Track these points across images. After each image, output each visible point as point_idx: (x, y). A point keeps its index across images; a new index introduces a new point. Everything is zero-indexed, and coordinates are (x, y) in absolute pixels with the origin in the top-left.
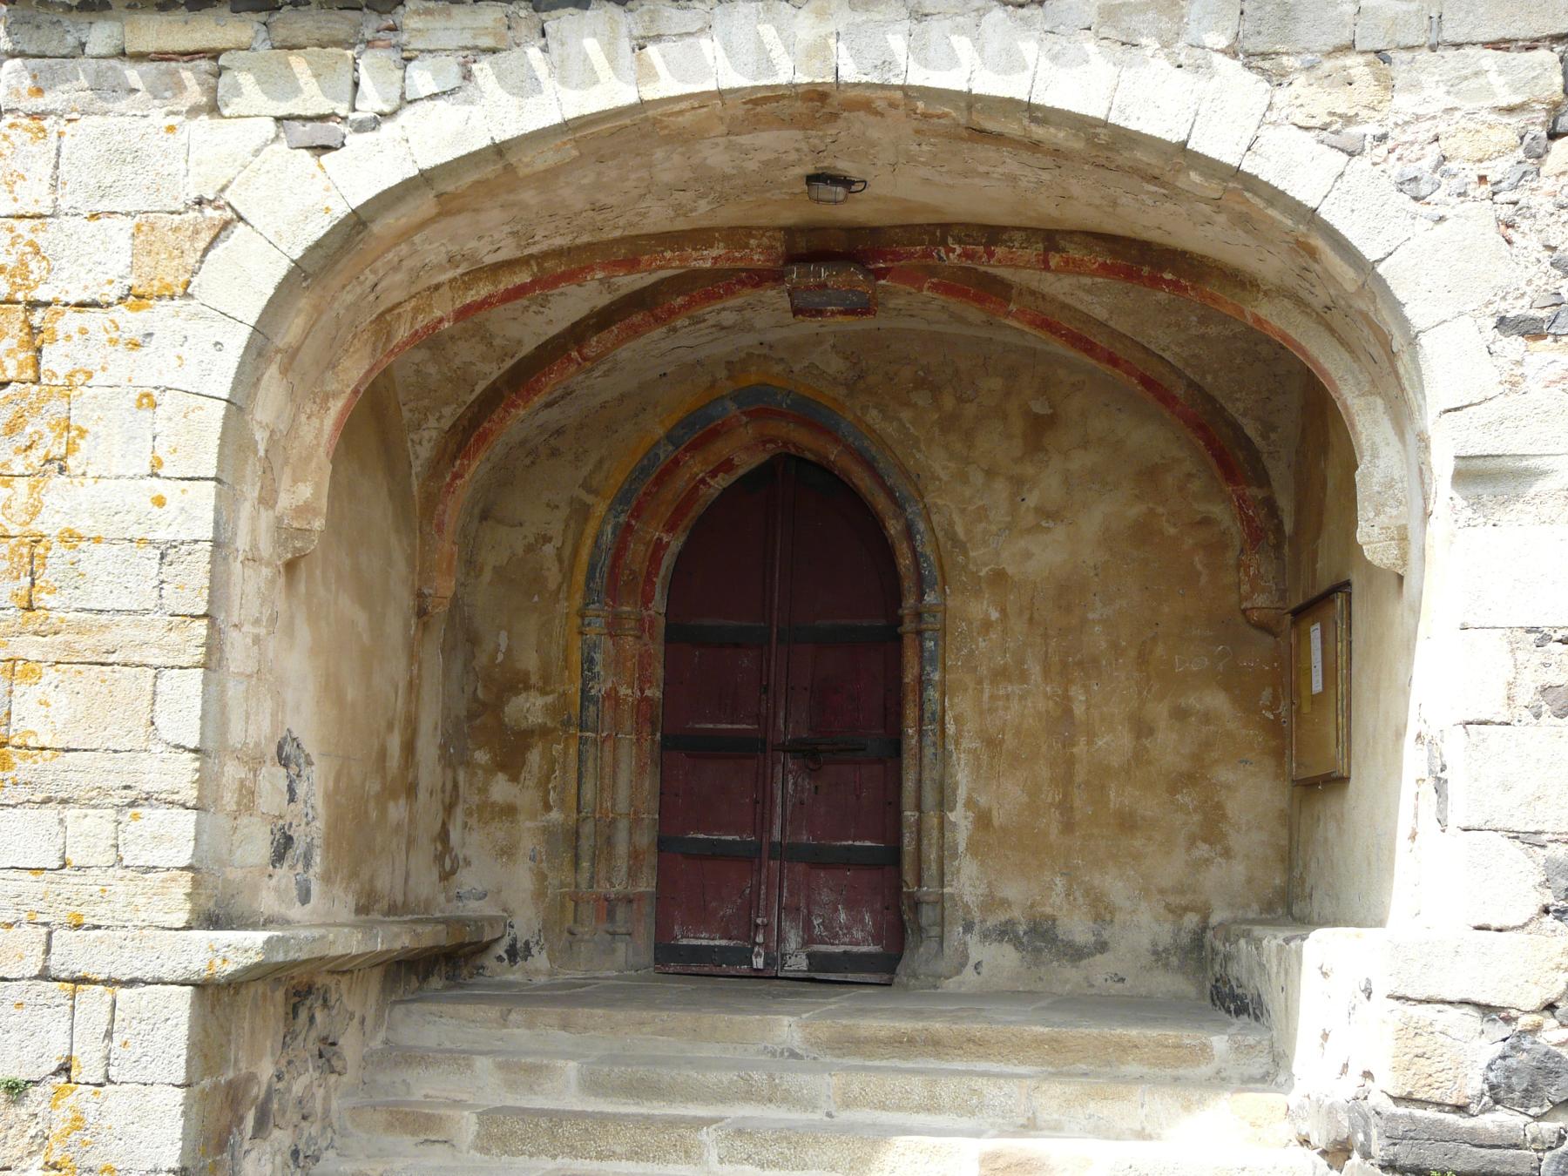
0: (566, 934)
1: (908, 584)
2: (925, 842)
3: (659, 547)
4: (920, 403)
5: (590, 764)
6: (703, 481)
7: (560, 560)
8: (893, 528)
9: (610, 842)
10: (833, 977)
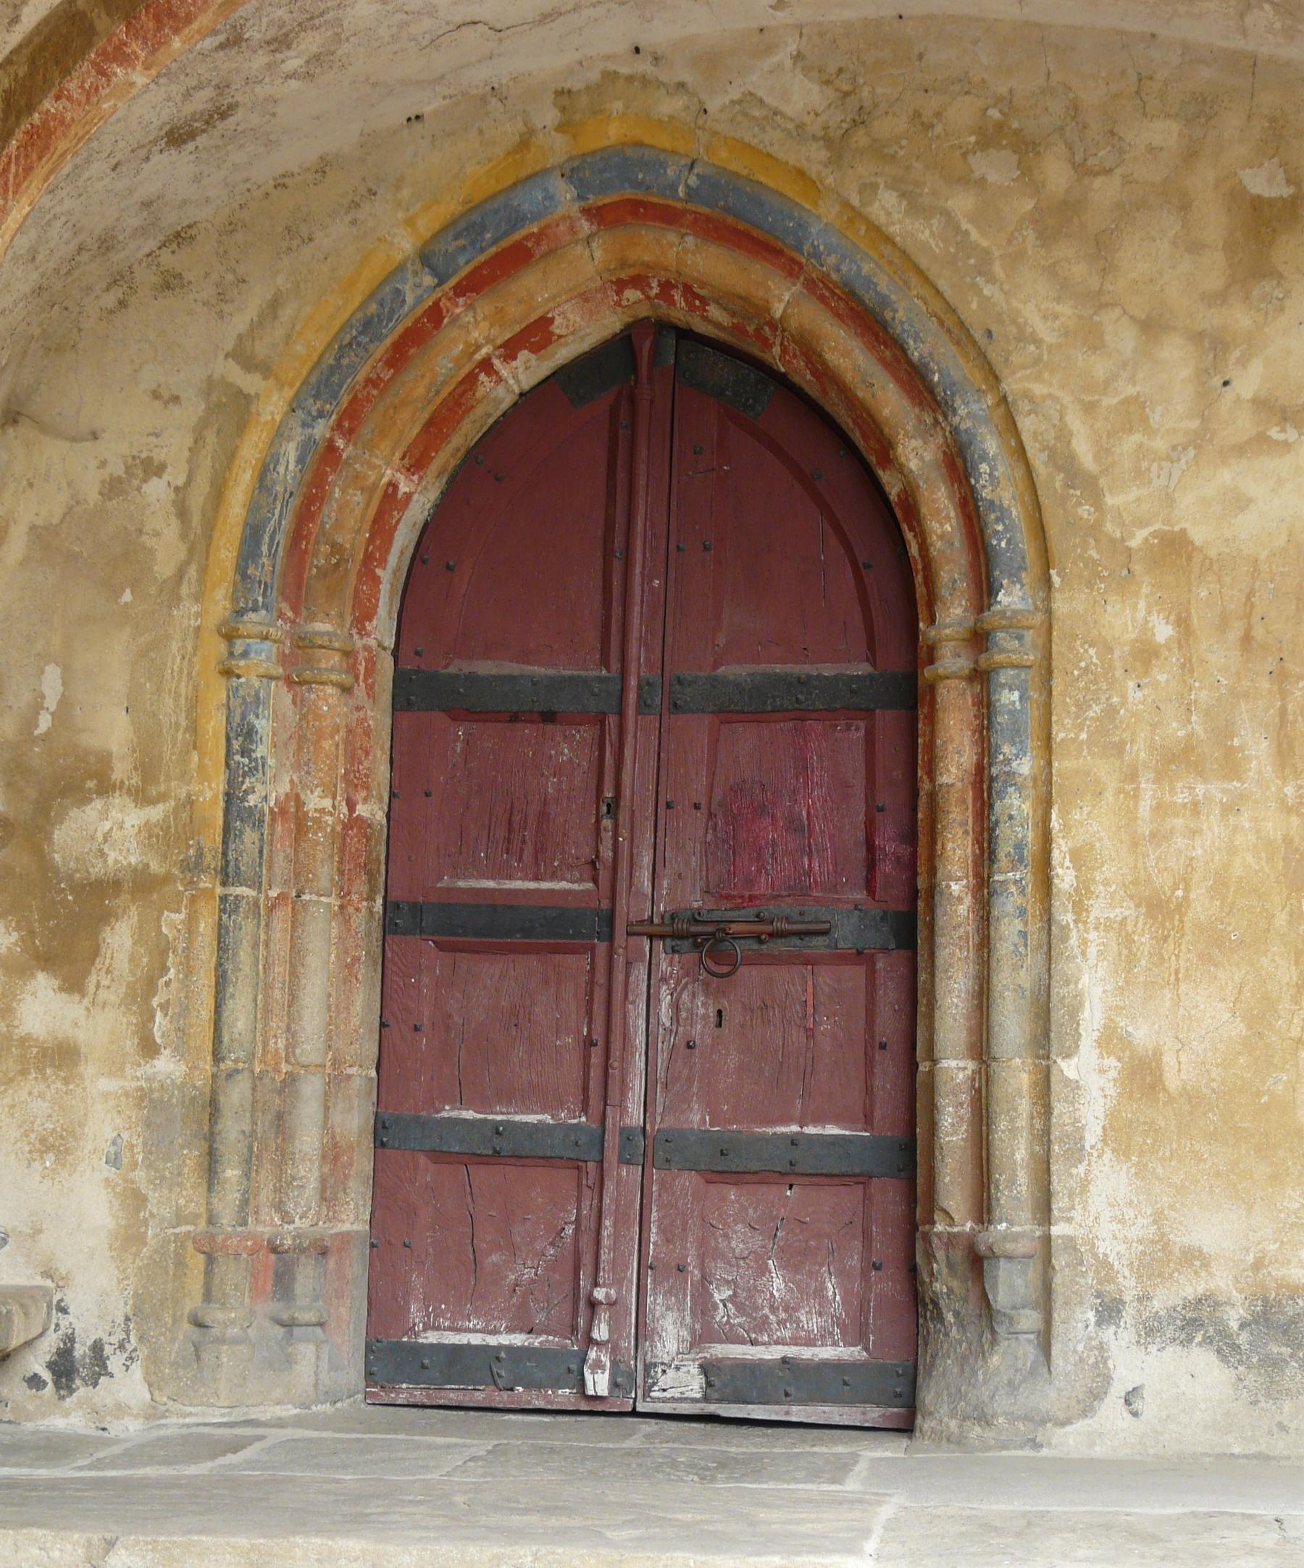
0: (186, 1326)
1: (952, 573)
2: (1002, 1124)
3: (391, 501)
4: (993, 177)
5: (244, 955)
6: (486, 365)
7: (182, 513)
8: (917, 454)
9: (281, 1122)
10: (758, 1412)
